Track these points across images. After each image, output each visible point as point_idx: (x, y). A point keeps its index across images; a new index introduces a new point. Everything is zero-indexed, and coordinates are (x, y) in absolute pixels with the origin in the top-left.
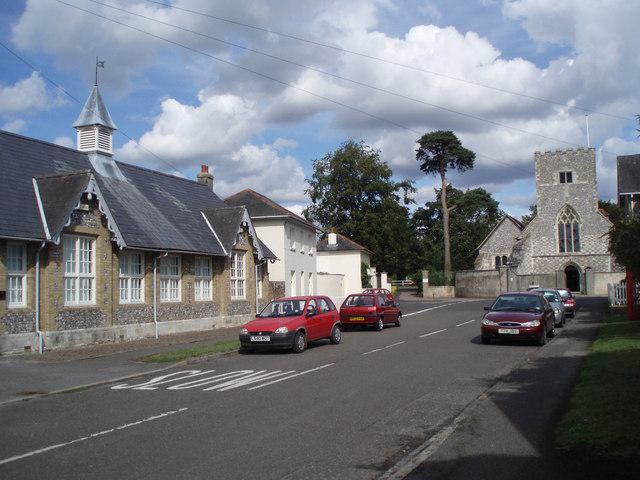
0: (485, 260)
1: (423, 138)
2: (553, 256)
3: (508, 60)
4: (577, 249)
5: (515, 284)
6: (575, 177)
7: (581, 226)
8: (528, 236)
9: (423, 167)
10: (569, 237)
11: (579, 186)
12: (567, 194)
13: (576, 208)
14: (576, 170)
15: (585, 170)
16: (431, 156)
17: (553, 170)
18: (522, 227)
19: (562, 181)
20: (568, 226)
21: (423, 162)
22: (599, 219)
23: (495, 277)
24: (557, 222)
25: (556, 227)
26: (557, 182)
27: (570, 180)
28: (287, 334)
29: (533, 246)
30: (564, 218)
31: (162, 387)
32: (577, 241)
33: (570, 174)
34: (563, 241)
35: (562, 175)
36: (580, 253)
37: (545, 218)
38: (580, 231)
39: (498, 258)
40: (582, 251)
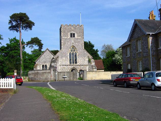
0: (38, 66)
1: (13, 15)
2: (67, 65)
3: (25, 14)
4: (76, 63)
5: (57, 76)
6: (76, 35)
7: (77, 54)
8: (58, 57)
9: (10, 27)
10: (73, 59)
11: (77, 39)
12: (73, 42)
13: (76, 47)
14: (76, 33)
15: (80, 33)
16: (14, 23)
17: (68, 32)
18: (55, 53)
19: (71, 36)
20: (73, 54)
21: (10, 26)
22: (84, 52)
23: (48, 73)
24: (69, 52)
25: (68, 54)
26: (69, 37)
27: (74, 36)
28: (6, 47)
29: (60, 61)
30: (72, 51)
31: (157, 88)
32: (76, 60)
33: (74, 34)
34: (71, 59)
35: (71, 34)
36: (77, 64)
37: (65, 50)
38: (77, 56)
39: (43, 66)
40: (78, 64)
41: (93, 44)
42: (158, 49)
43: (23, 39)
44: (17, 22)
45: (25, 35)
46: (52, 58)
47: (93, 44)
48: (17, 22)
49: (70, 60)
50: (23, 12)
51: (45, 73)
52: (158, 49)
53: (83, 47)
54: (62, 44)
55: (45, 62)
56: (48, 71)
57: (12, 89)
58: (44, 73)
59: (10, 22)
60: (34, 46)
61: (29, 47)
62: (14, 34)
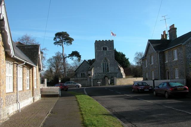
3: (66, 33)
4: (108, 71)
7: (109, 64)
11: (109, 52)
16: (58, 40)
20: (105, 64)
25: (102, 64)
26: (102, 50)
27: (106, 50)
30: (104, 61)
33: (106, 48)
35: (104, 48)
41: (127, 58)
42: (165, 63)
43: (48, 50)
44: (60, 38)
45: (68, 49)
46: (89, 67)
47: (127, 58)
48: (60, 38)
49: (103, 69)
50: (64, 31)
51: (83, 80)
52: (165, 63)
53: (114, 58)
54: (21, 42)
55: (83, 71)
56: (85, 78)
57: (58, 95)
58: (82, 80)
59: (55, 39)
60: (73, 57)
61: (70, 59)
62: (58, 49)
